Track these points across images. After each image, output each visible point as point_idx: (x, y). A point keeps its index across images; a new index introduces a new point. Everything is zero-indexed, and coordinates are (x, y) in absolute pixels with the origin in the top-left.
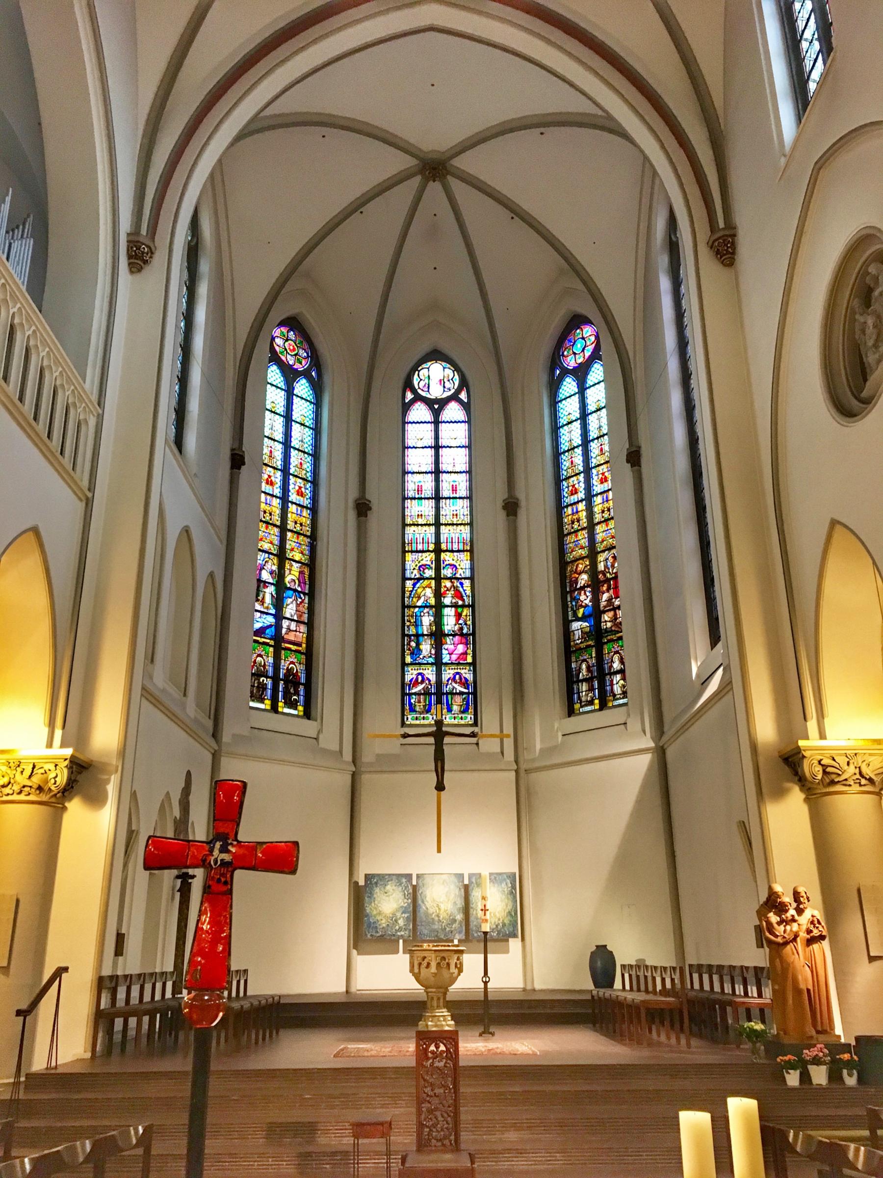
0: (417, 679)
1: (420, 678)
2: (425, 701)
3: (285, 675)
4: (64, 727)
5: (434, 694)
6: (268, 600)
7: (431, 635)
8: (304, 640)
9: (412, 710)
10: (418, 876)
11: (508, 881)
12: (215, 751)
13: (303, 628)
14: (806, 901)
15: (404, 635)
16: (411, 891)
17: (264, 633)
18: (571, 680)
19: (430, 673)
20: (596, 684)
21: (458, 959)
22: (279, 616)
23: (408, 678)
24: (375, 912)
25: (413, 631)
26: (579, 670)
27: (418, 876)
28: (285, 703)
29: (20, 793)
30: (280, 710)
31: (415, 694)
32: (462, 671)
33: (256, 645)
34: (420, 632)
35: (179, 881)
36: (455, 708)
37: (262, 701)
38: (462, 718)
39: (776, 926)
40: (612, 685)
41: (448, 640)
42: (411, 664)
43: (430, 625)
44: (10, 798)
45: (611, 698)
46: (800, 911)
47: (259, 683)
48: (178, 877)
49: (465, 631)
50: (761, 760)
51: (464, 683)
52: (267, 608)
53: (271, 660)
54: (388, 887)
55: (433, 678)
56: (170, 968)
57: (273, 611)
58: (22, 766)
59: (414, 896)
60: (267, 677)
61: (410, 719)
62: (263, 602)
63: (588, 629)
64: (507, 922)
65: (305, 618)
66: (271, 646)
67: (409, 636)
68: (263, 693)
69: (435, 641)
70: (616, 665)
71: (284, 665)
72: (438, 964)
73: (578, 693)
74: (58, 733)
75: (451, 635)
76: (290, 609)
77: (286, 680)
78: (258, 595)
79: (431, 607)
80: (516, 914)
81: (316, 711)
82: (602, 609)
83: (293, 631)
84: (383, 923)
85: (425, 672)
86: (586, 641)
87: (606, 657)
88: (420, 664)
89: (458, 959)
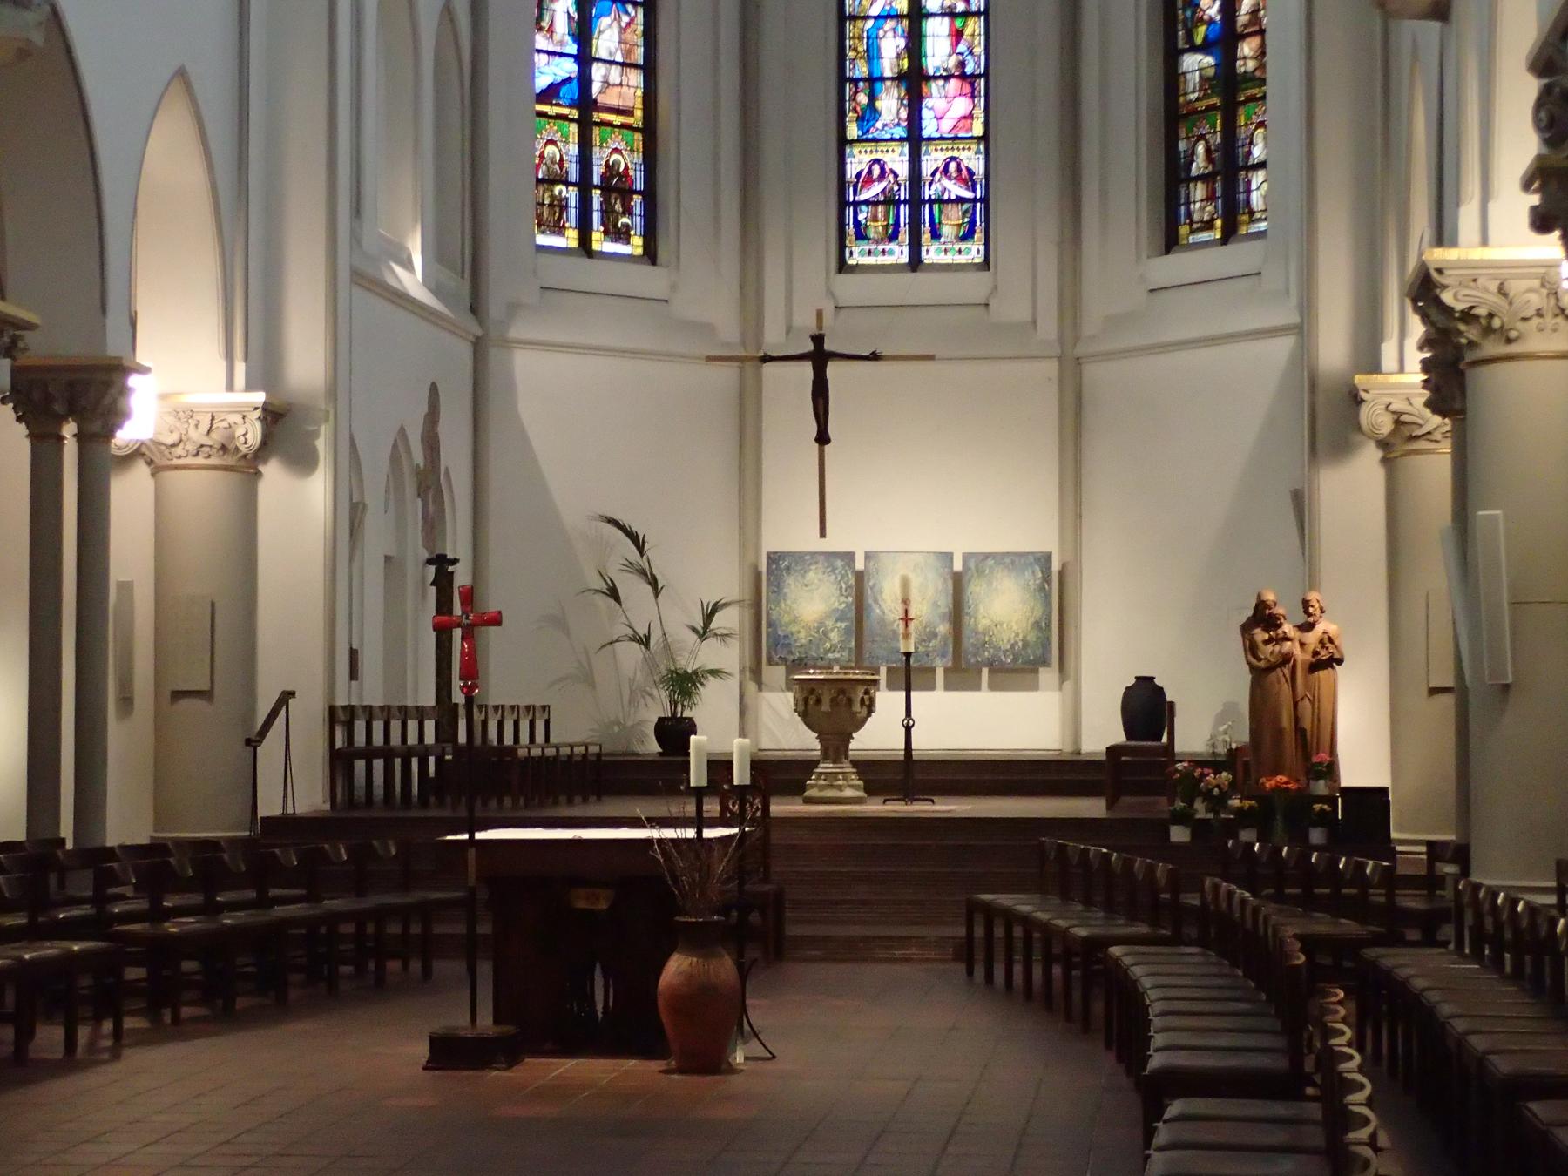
0: (870, 172)
1: (876, 170)
2: (886, 218)
3: (603, 177)
4: (246, 359)
5: (905, 202)
6: (562, 26)
7: (899, 78)
8: (639, 103)
9: (861, 235)
10: (868, 556)
11: (1037, 568)
12: (478, 338)
13: (636, 78)
14: (1318, 613)
15: (842, 79)
16: (852, 582)
17: (558, 96)
18: (1175, 175)
19: (897, 160)
20: (1218, 186)
21: (867, 692)
22: (585, 59)
23: (851, 172)
24: (786, 619)
25: (861, 70)
26: (1191, 155)
27: (868, 556)
28: (606, 233)
29: (197, 454)
30: (596, 246)
31: (867, 202)
32: (963, 155)
33: (543, 121)
34: (876, 74)
35: (432, 568)
36: (948, 231)
37: (559, 230)
38: (960, 251)
39: (1261, 645)
40: (1248, 191)
41: (935, 87)
42: (859, 140)
43: (898, 56)
44: (182, 462)
45: (1246, 218)
46: (1307, 627)
47: (553, 197)
48: (429, 562)
49: (969, 70)
50: (1321, 399)
51: (969, 180)
52: (561, 43)
53: (573, 149)
54: (811, 575)
55: (903, 170)
56: (428, 698)
57: (572, 48)
58: (197, 417)
59: (860, 590)
60: (567, 184)
61: (858, 254)
62: (551, 30)
63: (1211, 72)
64: (1032, 638)
65: (638, 56)
66: (572, 120)
67: (855, 81)
68: (560, 218)
69: (908, 92)
70: (1258, 152)
71: (600, 156)
72: (833, 700)
73: (1188, 203)
74: (240, 368)
75: (941, 77)
76: (607, 41)
77: (606, 188)
78: (540, 18)
79: (899, 17)
80: (1048, 625)
81: (663, 253)
82: (1239, 30)
83: (618, 87)
84: (803, 638)
85: (886, 157)
86: (1206, 96)
87: (1242, 133)
88: (875, 140)
89: (867, 692)
